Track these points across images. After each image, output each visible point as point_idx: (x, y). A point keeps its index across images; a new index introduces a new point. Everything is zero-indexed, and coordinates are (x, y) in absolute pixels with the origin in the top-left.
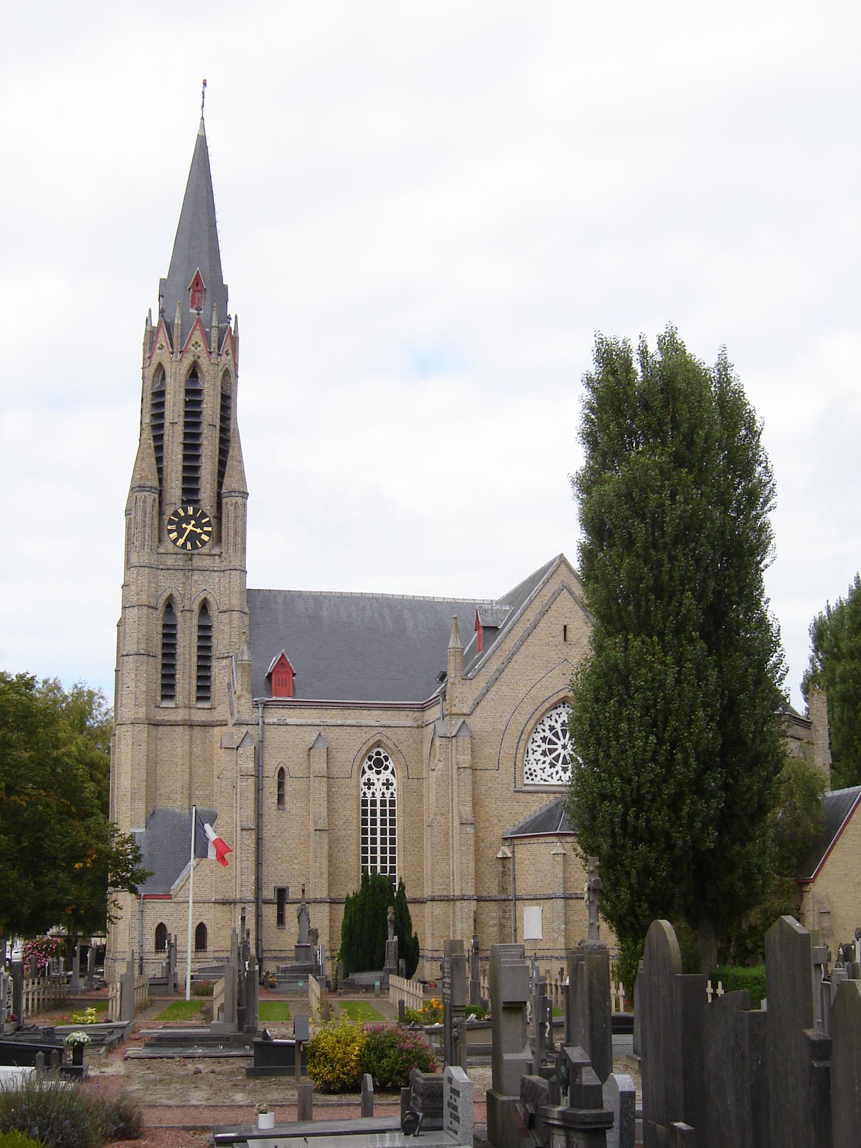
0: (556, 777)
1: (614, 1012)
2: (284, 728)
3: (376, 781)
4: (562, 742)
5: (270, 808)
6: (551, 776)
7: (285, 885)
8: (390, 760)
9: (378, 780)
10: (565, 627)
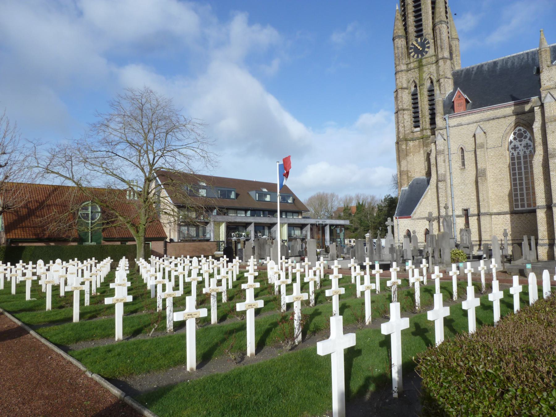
2: (460, 127)
3: (519, 146)
5: (440, 13)
7: (468, 207)
8: (528, 132)
9: (521, 145)
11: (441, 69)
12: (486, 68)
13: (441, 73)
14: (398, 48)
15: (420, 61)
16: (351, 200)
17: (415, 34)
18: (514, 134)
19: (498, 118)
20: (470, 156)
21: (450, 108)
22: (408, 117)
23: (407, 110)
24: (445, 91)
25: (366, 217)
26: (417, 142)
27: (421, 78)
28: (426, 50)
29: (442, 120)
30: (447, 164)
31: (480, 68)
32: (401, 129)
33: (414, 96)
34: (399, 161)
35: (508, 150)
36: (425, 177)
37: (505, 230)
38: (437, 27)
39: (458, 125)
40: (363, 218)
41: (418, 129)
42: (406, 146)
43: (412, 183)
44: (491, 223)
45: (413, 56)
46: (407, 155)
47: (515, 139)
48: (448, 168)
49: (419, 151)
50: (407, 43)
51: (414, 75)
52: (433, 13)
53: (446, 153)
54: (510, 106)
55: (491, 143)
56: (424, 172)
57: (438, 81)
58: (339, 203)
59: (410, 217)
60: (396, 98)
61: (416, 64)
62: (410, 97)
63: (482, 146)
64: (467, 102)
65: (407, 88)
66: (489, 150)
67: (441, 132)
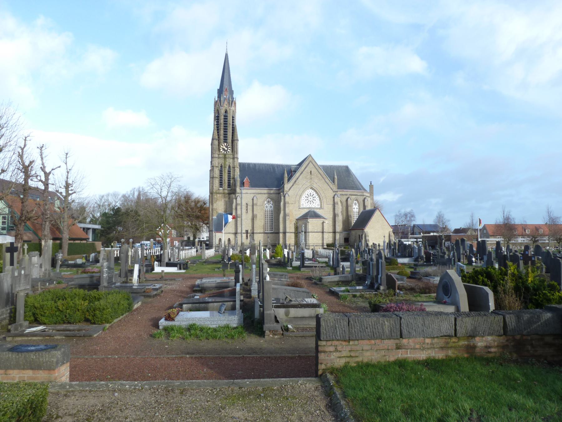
20: (250, 208)
22: (217, 182)
26: (221, 195)
27: (225, 164)
33: (221, 172)
41: (221, 188)
52: (232, 135)
55: (258, 204)
63: (256, 205)
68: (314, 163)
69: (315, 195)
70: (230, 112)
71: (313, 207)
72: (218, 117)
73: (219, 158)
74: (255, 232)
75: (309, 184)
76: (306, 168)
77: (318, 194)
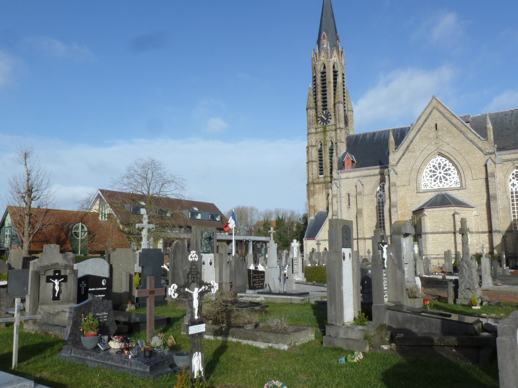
0: (437, 186)
1: (238, 294)
4: (439, 171)
5: (339, 95)
6: (435, 185)
10: (436, 124)
11: (338, 135)
12: (368, 136)
13: (338, 138)
14: (310, 116)
15: (325, 128)
16: (271, 214)
17: (322, 107)
18: (380, 187)
19: (371, 176)
21: (342, 166)
22: (315, 167)
23: (315, 162)
24: (340, 151)
25: (286, 232)
26: (321, 186)
27: (325, 140)
28: (329, 120)
29: (336, 174)
30: (339, 204)
31: (365, 135)
32: (311, 176)
33: (320, 151)
34: (309, 198)
35: (376, 197)
36: (326, 211)
37: (369, 250)
38: (336, 105)
39: (347, 178)
40: (283, 233)
41: (322, 176)
42: (314, 188)
43: (318, 214)
44: (365, 245)
45: (320, 123)
46: (314, 194)
47: (380, 190)
48: (339, 206)
49: (323, 192)
50: (316, 112)
51: (320, 137)
53: (339, 196)
54: (377, 169)
55: (366, 192)
56: (325, 207)
57: (336, 143)
58: (259, 217)
59: (314, 239)
60: (308, 152)
61: (322, 129)
62: (317, 153)
63: (360, 194)
64: (353, 162)
65: (315, 146)
66: (365, 196)
67: (336, 181)
68: (442, 109)
69: (449, 165)
70: (329, 66)
71: (446, 187)
72: (315, 77)
73: (316, 133)
74: (494, 229)
75: (433, 148)
76: (426, 121)
77: (454, 164)
